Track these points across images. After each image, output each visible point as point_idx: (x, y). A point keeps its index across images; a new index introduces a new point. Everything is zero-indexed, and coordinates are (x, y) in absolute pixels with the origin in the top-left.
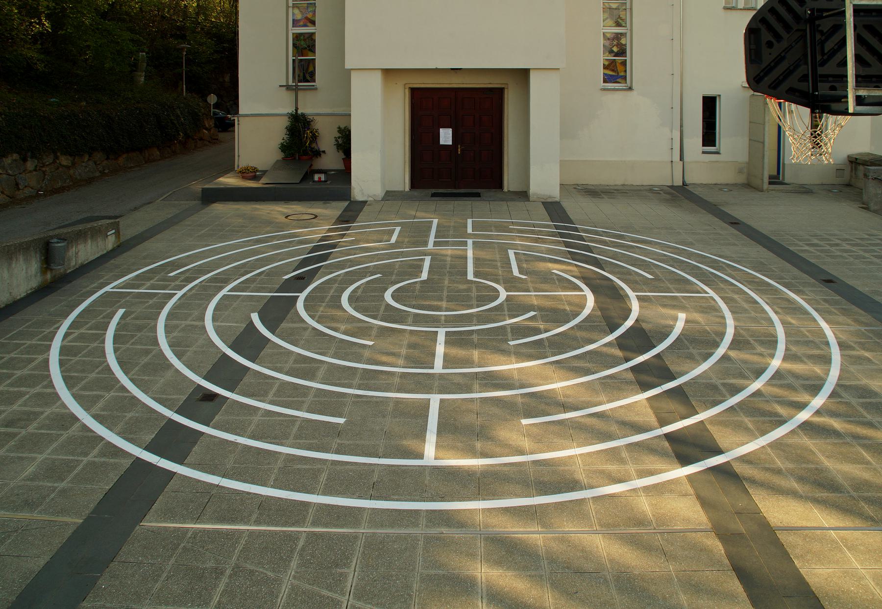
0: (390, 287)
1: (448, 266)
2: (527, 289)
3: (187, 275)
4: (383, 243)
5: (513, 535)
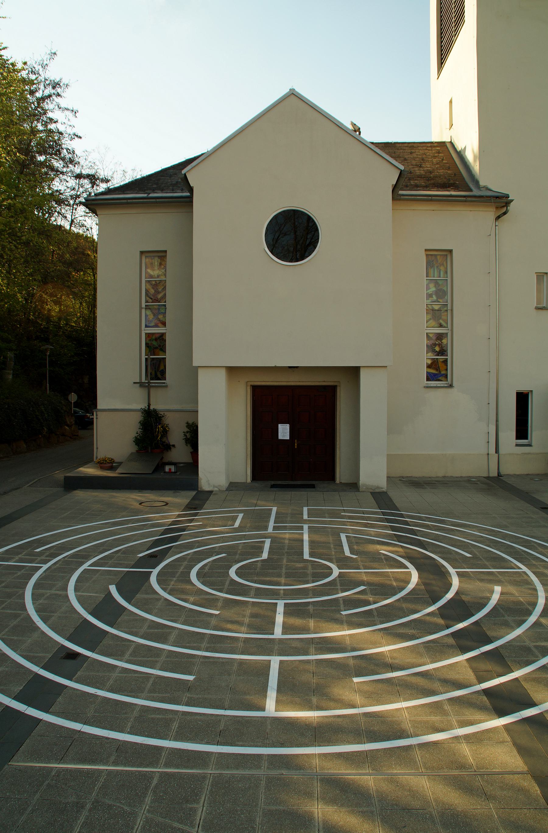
0: (234, 565)
1: (286, 547)
2: (358, 567)
3: (52, 551)
4: (229, 527)
5: (347, 776)
